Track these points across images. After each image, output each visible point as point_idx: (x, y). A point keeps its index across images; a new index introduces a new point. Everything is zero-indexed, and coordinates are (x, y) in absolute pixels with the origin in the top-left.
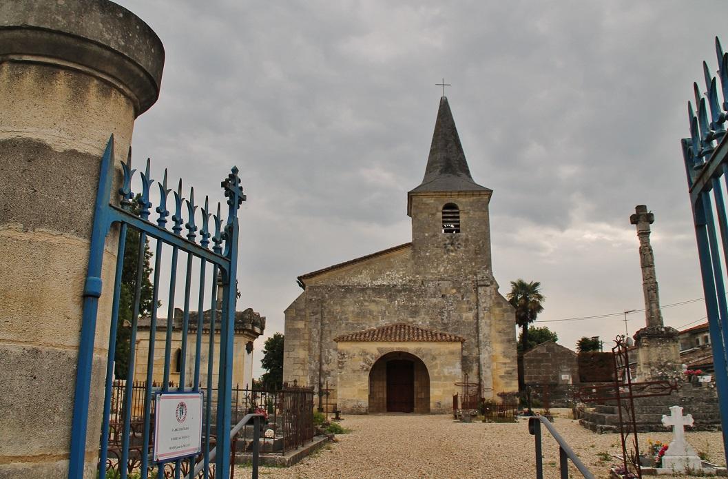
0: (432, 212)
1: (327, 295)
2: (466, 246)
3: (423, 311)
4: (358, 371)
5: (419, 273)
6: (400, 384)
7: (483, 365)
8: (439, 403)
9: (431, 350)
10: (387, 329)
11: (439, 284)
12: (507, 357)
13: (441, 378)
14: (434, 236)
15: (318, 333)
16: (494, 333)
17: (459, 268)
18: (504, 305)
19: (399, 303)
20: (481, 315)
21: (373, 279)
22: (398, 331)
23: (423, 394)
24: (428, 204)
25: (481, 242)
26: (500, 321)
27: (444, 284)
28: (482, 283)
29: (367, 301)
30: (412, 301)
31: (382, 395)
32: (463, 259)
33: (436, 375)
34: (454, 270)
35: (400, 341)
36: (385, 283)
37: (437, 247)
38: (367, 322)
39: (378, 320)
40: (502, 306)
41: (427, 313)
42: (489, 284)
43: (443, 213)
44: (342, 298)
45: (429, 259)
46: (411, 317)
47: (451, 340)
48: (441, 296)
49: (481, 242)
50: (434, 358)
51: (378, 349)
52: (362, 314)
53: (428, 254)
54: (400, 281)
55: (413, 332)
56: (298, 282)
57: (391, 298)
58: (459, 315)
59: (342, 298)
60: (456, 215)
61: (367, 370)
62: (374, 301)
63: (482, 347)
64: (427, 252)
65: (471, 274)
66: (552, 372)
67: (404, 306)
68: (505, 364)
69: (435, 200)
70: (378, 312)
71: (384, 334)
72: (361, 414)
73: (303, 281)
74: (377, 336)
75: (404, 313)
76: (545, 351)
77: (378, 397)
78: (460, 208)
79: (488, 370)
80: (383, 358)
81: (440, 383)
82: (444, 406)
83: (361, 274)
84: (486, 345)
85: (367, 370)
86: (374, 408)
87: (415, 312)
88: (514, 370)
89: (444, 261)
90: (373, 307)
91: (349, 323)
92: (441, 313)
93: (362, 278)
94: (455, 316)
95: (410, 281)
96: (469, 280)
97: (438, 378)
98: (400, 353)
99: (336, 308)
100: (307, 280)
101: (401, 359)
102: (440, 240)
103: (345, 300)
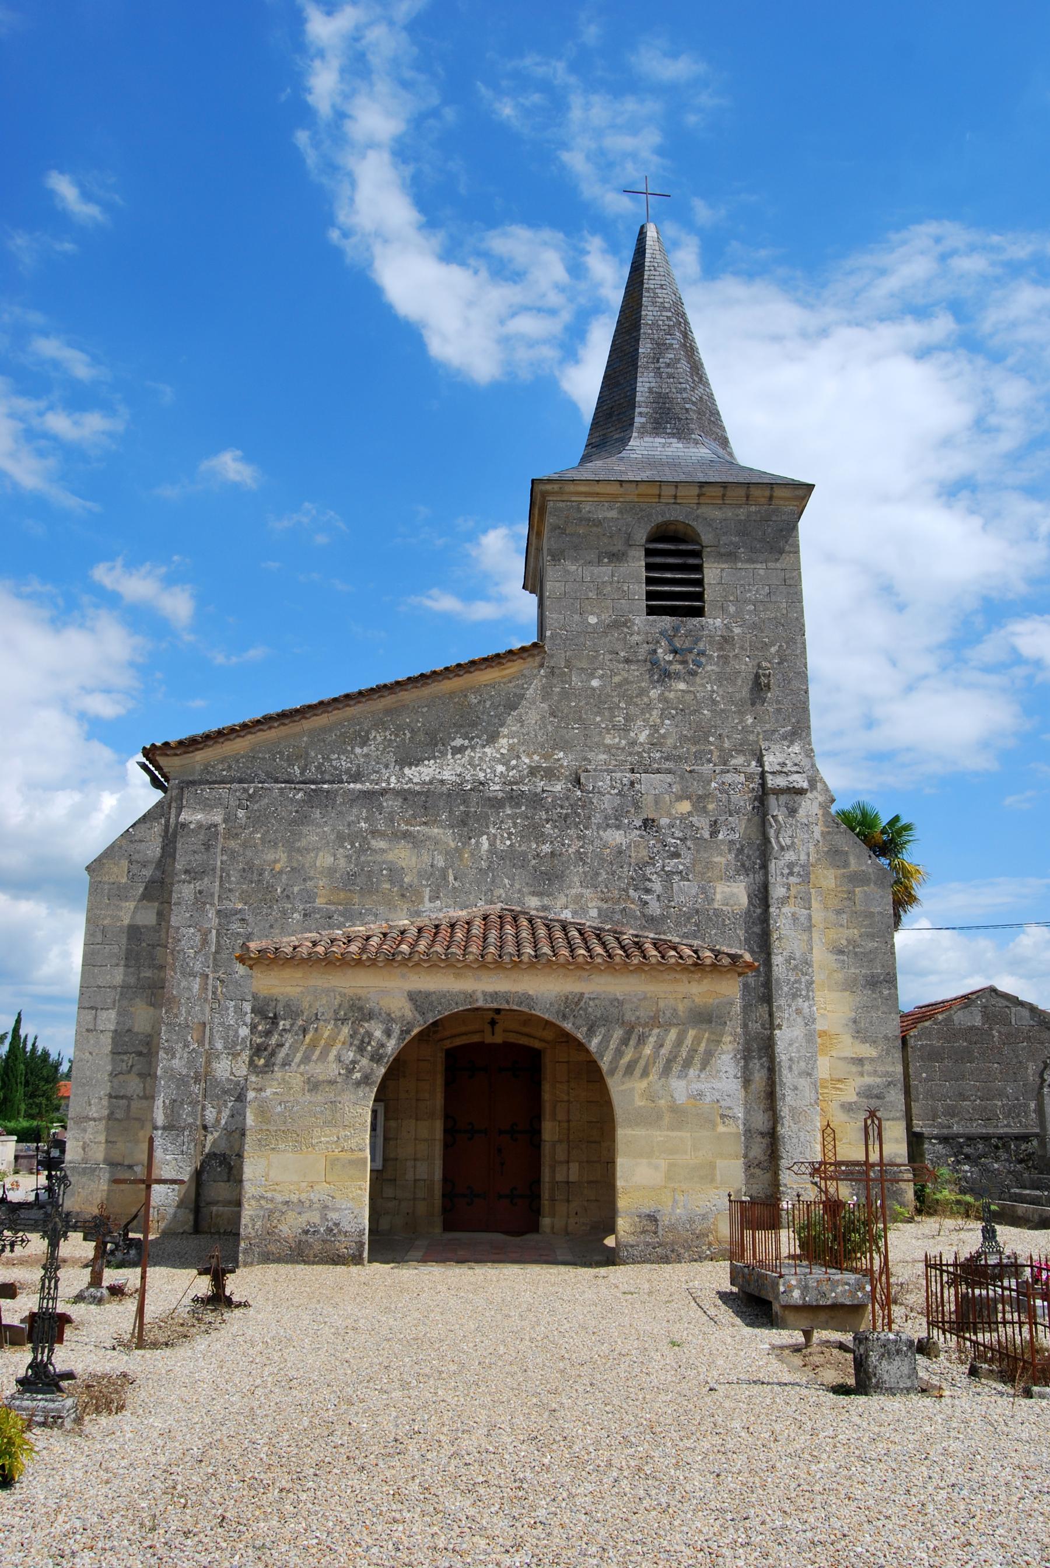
0: (615, 549)
1: (241, 813)
2: (724, 659)
3: (576, 873)
4: (332, 1082)
5: (565, 745)
6: (494, 1145)
7: (785, 1064)
8: (652, 1218)
9: (621, 1003)
10: (452, 926)
11: (632, 784)
12: (864, 1040)
13: (660, 1117)
14: (616, 625)
15: (205, 942)
16: (820, 955)
17: (700, 735)
18: (852, 861)
19: (492, 844)
20: (778, 891)
21: (408, 760)
22: (493, 935)
23: (574, 1167)
24: (598, 523)
25: (773, 650)
26: (839, 912)
27: (651, 784)
28: (781, 782)
29: (382, 835)
30: (541, 838)
31: (427, 1165)
32: (714, 702)
33: (639, 1102)
34: (683, 739)
35: (498, 964)
36: (447, 775)
37: (627, 661)
38: (381, 909)
39: (422, 902)
40: (846, 865)
41: (591, 880)
42: (805, 785)
43: (649, 553)
44: (294, 822)
45: (599, 701)
46: (533, 894)
47: (698, 965)
48: (638, 823)
49: (773, 650)
50: (634, 1034)
51: (413, 997)
52: (361, 881)
53: (595, 683)
54: (500, 768)
55: (550, 938)
56: (144, 767)
57: (467, 825)
58: (703, 890)
59: (294, 822)
60: (691, 561)
61: (366, 1080)
62: (406, 835)
63: (782, 1002)
64: (592, 676)
65: (739, 752)
66: (1001, 1094)
67: (513, 858)
68: (860, 1061)
69: (621, 512)
70: (420, 875)
71: (440, 946)
72: (337, 1260)
73: (162, 761)
74: (413, 946)
75: (512, 879)
76: (978, 1021)
77: (410, 1176)
78: (707, 538)
79: (803, 1083)
80: (430, 1033)
81: (658, 1135)
82: (672, 1228)
83: (364, 743)
84: (795, 996)
85: (366, 1080)
86: (392, 1237)
87: (548, 877)
88: (890, 1084)
89: (649, 707)
90: (402, 855)
91: (316, 910)
92: (641, 883)
93: (366, 755)
94: (686, 892)
95: (533, 771)
96: (737, 771)
97: (651, 1118)
98: (494, 1017)
99: (270, 856)
100: (176, 761)
101: (498, 1039)
102: (636, 638)
103: (305, 830)
